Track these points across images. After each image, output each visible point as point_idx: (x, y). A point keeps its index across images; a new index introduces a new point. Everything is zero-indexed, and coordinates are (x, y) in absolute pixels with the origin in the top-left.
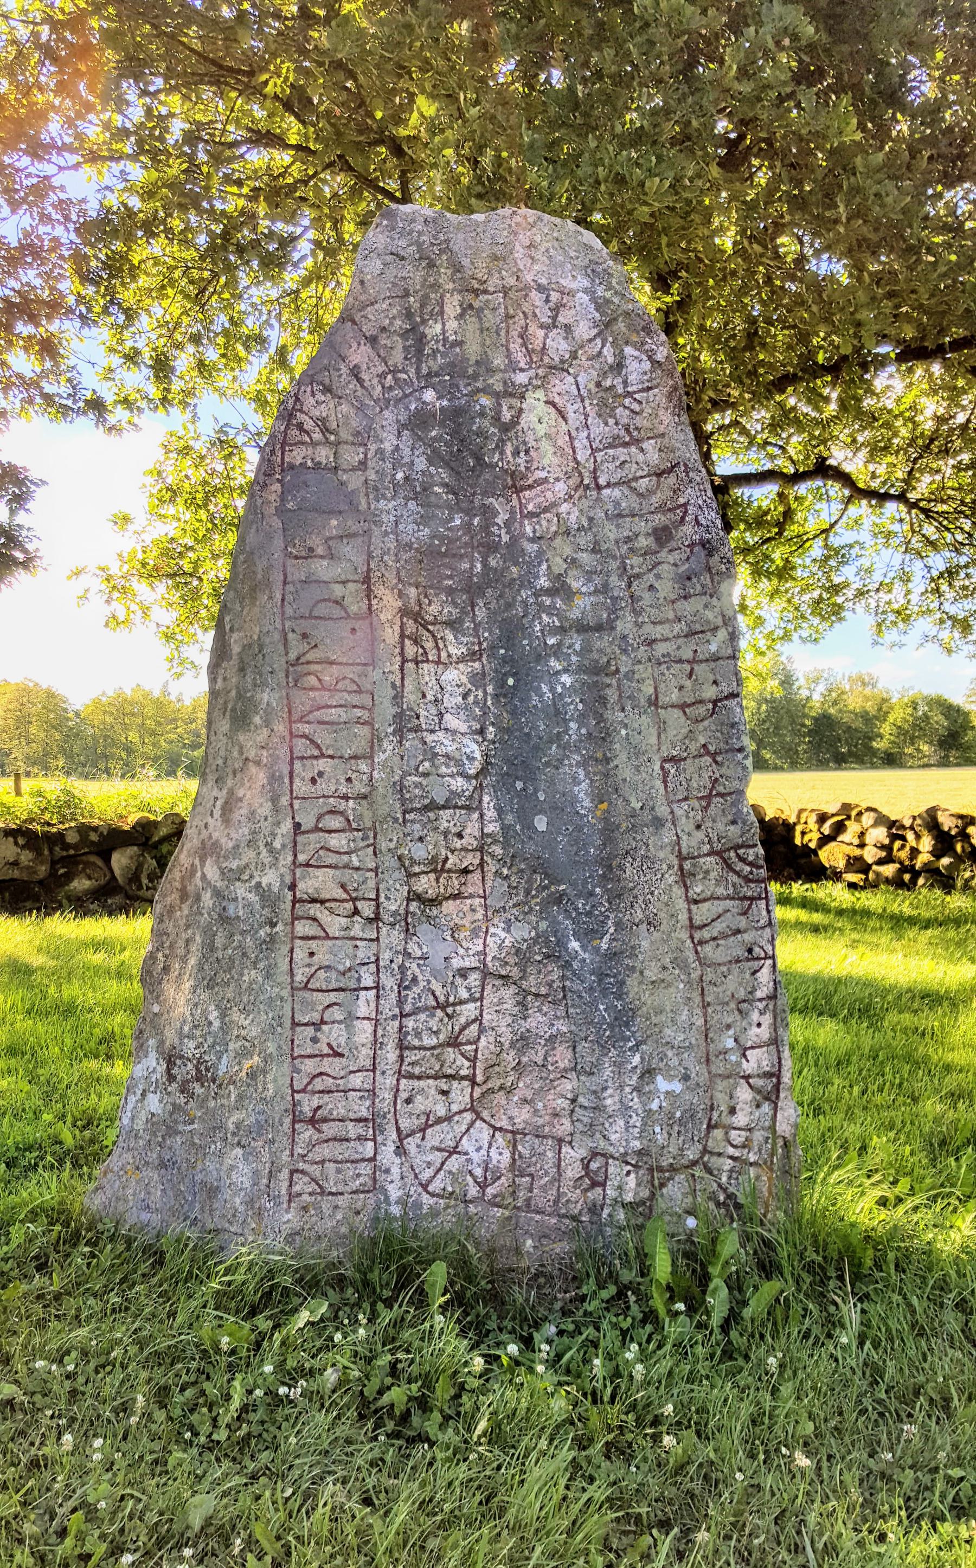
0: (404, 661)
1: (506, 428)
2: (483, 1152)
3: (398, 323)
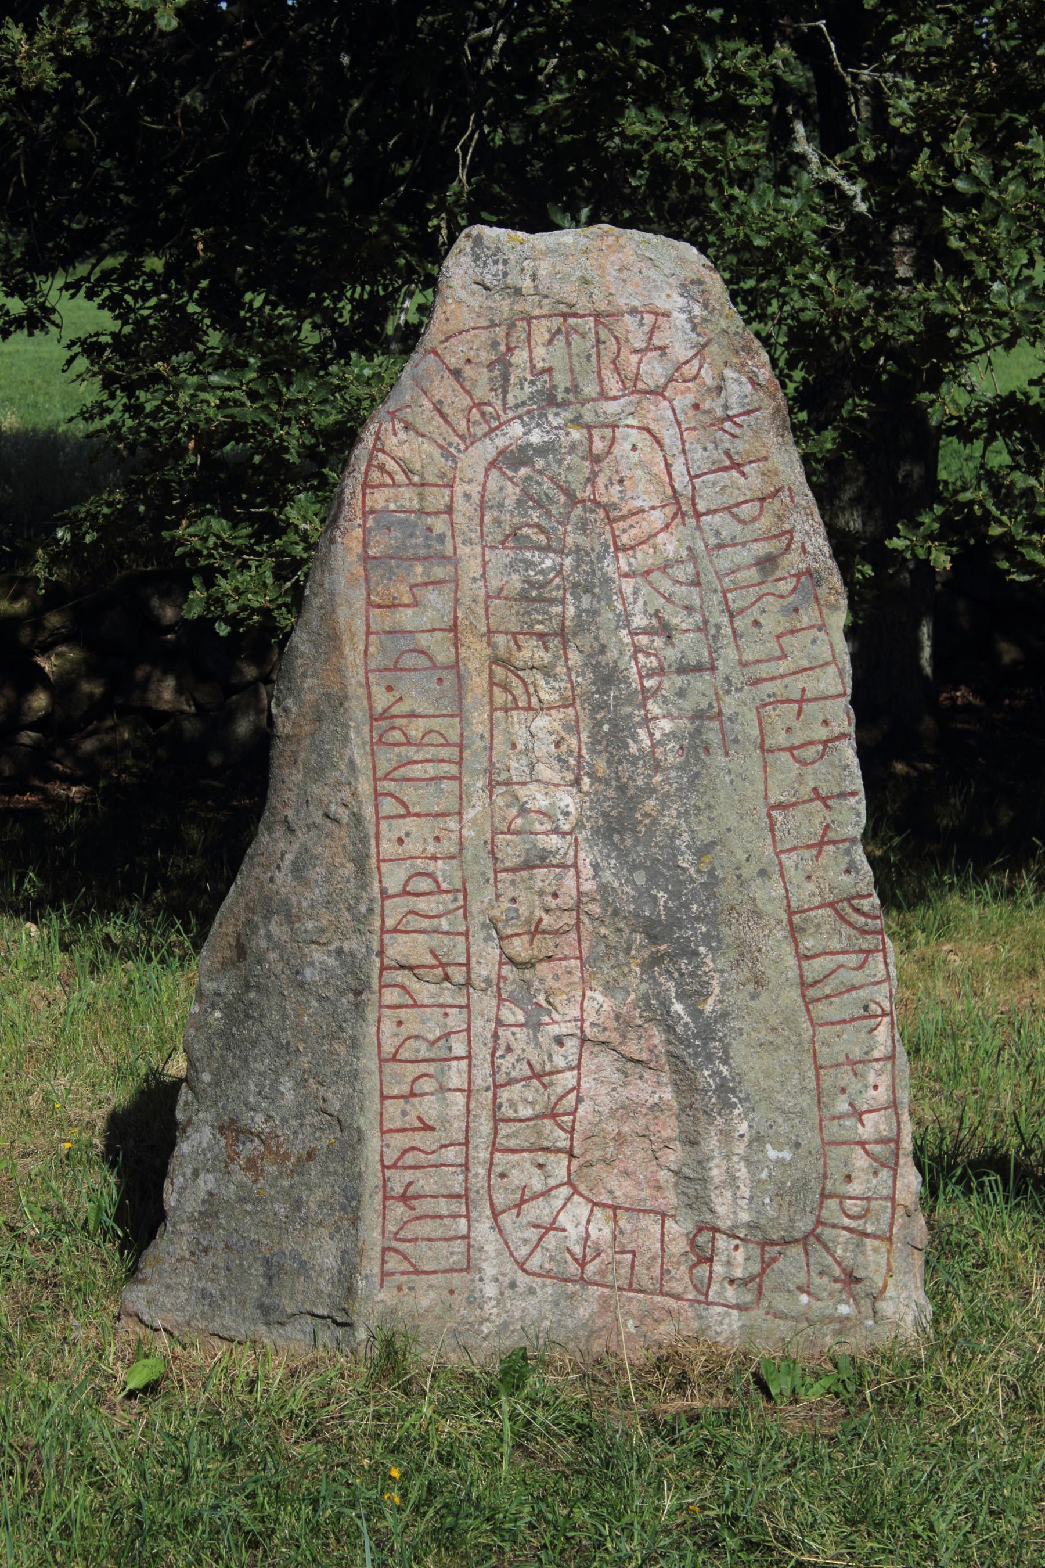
0: (493, 710)
1: (596, 459)
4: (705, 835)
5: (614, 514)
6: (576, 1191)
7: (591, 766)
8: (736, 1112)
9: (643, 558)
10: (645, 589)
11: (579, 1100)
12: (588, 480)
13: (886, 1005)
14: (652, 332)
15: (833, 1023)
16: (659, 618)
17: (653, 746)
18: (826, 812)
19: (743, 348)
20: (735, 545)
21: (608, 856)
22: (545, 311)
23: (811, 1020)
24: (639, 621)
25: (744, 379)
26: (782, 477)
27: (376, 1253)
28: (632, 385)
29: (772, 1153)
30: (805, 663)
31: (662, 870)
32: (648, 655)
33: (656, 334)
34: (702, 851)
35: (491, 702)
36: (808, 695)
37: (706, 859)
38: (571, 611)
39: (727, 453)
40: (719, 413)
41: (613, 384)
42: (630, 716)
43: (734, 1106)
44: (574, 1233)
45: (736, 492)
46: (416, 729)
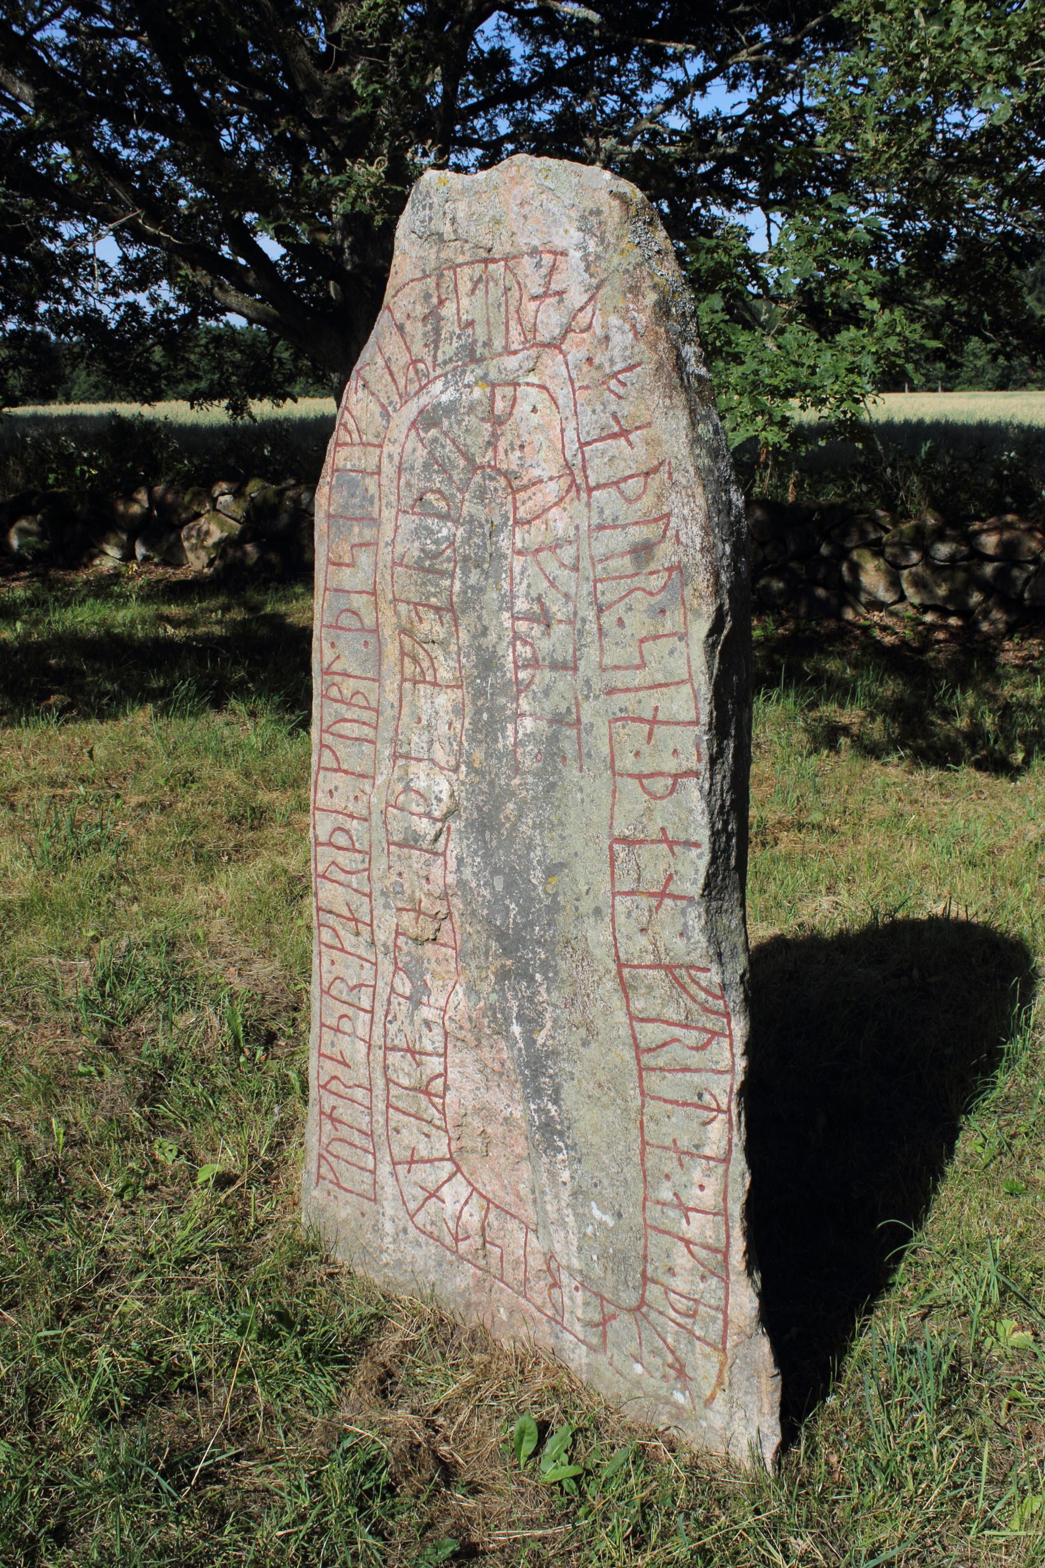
0: (404, 680)
1: (499, 422)
2: (458, 1207)
4: (555, 855)
5: (516, 483)
6: (459, 1169)
7: (469, 755)
8: (560, 1157)
9: (534, 535)
10: (533, 569)
11: (446, 1088)
12: (489, 443)
13: (724, 1101)
14: (550, 274)
15: (665, 1101)
16: (542, 605)
17: (515, 745)
18: (671, 859)
20: (615, 527)
21: (476, 852)
22: (467, 258)
23: (641, 1086)
24: (521, 605)
26: (665, 448)
27: (313, 1155)
29: (597, 1213)
30: (660, 678)
31: (515, 881)
32: (525, 643)
34: (552, 870)
35: (402, 672)
36: (660, 716)
37: (554, 881)
38: (457, 586)
39: (614, 416)
42: (504, 708)
43: (560, 1151)
44: (450, 1208)
45: (622, 464)
46: (349, 686)
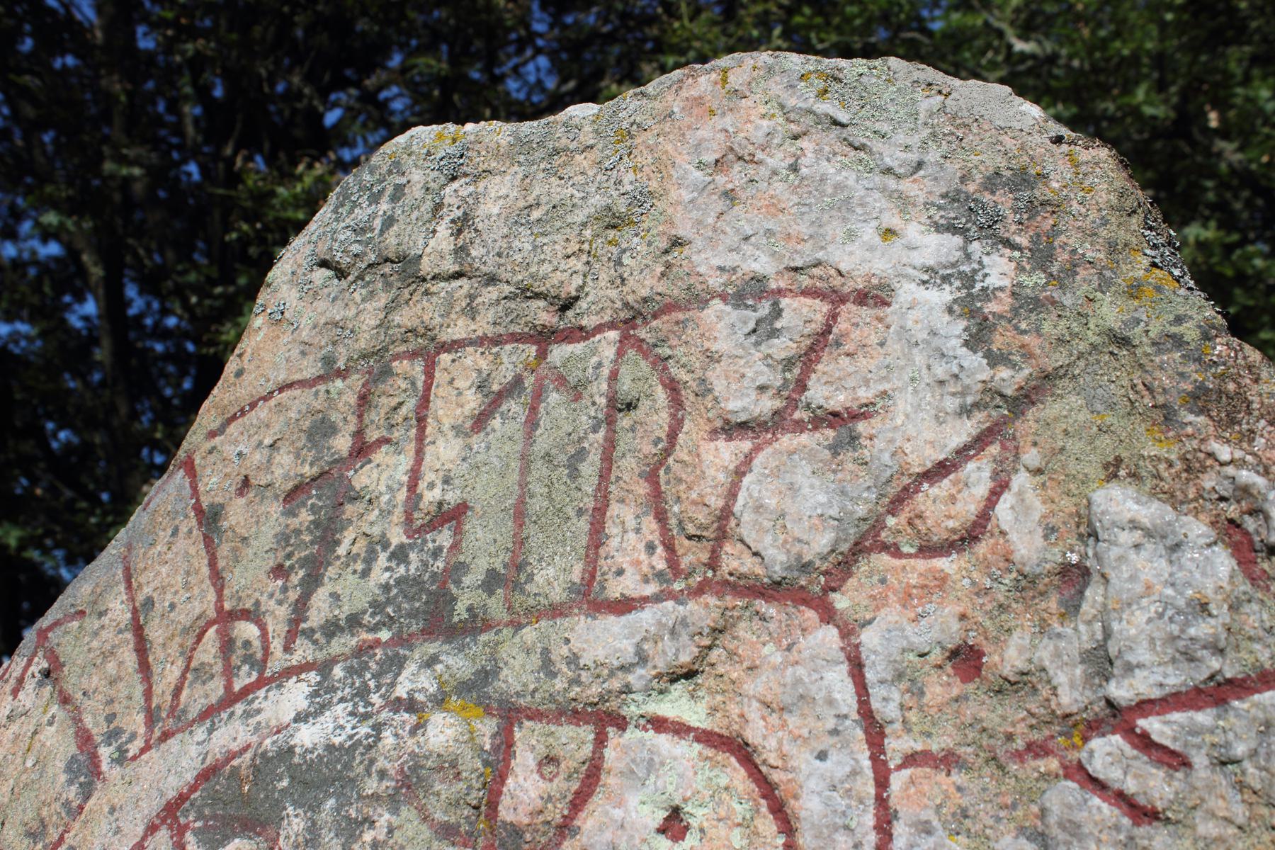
3: (284, 459)
19: (1199, 399)
22: (483, 326)
25: (1197, 529)
28: (703, 558)
33: (825, 366)
40: (1070, 692)
41: (631, 552)
